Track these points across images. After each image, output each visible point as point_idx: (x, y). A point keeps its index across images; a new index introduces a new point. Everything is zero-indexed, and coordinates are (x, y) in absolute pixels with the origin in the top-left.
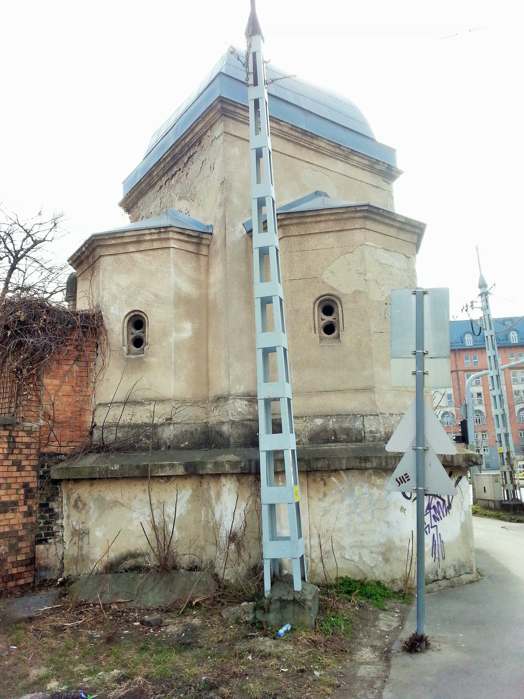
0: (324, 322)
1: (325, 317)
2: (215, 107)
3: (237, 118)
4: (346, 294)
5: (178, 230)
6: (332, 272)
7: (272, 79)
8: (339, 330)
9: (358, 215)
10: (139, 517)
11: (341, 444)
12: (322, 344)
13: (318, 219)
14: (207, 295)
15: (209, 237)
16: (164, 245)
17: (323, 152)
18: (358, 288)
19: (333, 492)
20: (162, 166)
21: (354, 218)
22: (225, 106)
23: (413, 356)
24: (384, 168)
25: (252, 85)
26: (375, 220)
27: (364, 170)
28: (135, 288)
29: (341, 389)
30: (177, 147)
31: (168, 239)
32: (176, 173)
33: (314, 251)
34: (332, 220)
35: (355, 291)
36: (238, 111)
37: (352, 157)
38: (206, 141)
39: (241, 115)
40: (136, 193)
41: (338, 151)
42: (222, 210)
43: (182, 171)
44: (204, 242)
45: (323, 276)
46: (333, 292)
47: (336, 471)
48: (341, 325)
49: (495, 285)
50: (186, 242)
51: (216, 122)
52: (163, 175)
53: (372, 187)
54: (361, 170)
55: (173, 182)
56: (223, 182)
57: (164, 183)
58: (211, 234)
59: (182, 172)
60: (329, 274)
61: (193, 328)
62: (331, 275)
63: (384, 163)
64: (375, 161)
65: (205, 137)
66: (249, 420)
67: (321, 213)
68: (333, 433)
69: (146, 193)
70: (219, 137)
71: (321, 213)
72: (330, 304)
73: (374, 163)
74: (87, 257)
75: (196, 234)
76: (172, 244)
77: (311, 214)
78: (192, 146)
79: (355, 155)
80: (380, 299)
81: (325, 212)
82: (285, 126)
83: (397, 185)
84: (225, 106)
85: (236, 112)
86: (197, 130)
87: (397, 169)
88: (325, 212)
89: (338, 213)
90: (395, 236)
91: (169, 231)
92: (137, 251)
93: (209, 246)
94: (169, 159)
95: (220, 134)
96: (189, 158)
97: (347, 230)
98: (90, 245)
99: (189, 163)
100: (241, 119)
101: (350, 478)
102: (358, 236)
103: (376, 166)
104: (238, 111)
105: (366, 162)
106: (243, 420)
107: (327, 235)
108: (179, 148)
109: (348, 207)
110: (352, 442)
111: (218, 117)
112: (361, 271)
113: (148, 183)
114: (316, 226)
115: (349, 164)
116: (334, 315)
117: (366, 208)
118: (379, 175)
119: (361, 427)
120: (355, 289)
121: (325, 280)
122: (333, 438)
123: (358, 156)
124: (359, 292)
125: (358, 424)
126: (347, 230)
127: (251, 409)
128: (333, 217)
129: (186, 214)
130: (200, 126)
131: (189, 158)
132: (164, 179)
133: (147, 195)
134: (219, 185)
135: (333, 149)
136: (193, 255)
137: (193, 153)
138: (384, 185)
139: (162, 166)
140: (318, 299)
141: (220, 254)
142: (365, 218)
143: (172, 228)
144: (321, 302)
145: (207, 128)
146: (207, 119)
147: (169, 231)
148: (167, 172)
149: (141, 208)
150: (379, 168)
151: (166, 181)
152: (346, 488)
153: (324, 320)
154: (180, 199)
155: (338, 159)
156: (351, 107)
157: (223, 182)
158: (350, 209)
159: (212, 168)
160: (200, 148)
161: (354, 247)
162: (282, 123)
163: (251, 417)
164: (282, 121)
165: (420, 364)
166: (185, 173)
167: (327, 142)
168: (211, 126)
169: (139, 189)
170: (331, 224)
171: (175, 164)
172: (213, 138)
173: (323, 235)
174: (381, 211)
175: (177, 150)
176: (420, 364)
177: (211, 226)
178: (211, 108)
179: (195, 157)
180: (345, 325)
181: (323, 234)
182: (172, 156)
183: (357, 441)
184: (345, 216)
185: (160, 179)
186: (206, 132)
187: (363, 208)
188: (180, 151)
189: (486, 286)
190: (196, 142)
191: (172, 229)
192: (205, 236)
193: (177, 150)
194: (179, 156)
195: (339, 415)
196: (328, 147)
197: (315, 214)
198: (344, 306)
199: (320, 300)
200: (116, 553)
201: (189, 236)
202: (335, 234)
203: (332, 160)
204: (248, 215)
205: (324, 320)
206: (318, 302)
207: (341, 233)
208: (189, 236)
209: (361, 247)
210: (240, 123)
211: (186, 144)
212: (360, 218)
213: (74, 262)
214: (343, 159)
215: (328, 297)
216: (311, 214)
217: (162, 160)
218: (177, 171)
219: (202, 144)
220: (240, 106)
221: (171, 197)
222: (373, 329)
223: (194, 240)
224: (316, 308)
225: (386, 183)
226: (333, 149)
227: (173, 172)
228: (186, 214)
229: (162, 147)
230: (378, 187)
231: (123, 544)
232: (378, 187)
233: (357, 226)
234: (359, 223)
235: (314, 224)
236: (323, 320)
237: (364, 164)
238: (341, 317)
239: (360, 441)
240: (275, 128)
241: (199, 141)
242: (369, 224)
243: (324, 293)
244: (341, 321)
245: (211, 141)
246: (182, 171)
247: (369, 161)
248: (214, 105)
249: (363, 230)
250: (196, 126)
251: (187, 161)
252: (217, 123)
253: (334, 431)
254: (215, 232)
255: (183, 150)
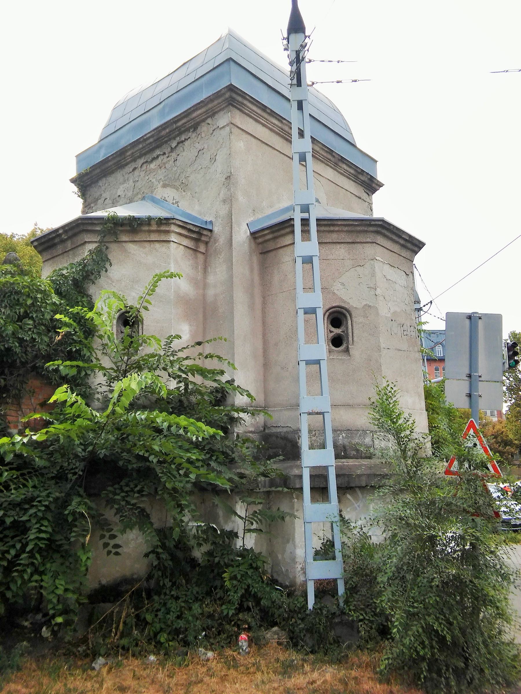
0: (332, 334)
1: (333, 329)
2: (224, 94)
3: (243, 109)
4: (356, 308)
5: (180, 223)
6: (343, 284)
7: (314, 81)
8: (348, 342)
9: (371, 229)
10: (137, 538)
11: (352, 460)
12: (331, 357)
13: (332, 228)
14: (204, 296)
15: (209, 233)
16: (163, 237)
17: (316, 156)
18: (368, 303)
19: (349, 510)
20: (141, 146)
21: (366, 231)
22: (234, 96)
23: (467, 378)
24: (366, 179)
25: (295, 85)
26: (385, 236)
27: (349, 179)
28: (128, 282)
29: (351, 403)
30: (164, 129)
31: (168, 232)
32: (158, 157)
33: (325, 261)
34: (345, 231)
35: (366, 305)
36: (245, 102)
37: (341, 164)
38: (204, 128)
39: (248, 107)
40: (98, 171)
41: (329, 157)
42: (227, 207)
43: (167, 155)
44: (203, 238)
45: (333, 287)
46: (343, 305)
47: (351, 488)
48: (350, 339)
49: (431, 302)
50: (186, 237)
51: (220, 110)
52: (140, 157)
53: (355, 197)
54: (346, 179)
55: (152, 166)
56: (230, 177)
57: (140, 166)
58: (211, 231)
59: (168, 157)
60: (340, 285)
61: (191, 331)
62: (342, 287)
63: (368, 174)
64: (360, 171)
65: (203, 124)
66: (251, 432)
67: (336, 223)
68: (343, 449)
69: (112, 172)
70: (223, 127)
71: (336, 223)
72: (339, 316)
73: (359, 173)
74: (63, 241)
75: (197, 230)
76: (173, 237)
77: (326, 223)
78: (185, 131)
79: (344, 163)
80: (386, 315)
81: (339, 223)
82: (286, 125)
83: (376, 197)
84: (234, 96)
85: (243, 104)
86: (194, 115)
87: (378, 181)
88: (339, 223)
89: (352, 225)
90: (398, 253)
91: (171, 223)
92: (130, 241)
93: (207, 243)
94: (151, 140)
95: (225, 124)
96: (178, 143)
97: (358, 243)
98: (72, 228)
99: (178, 148)
100: (247, 112)
101: (365, 495)
102: (369, 250)
103: (360, 176)
104: (245, 102)
105: (352, 171)
106: (246, 432)
107: (338, 246)
108: (167, 130)
109: (362, 220)
110: (362, 458)
111: (224, 105)
112: (372, 286)
113: (117, 162)
114: (329, 235)
115: (337, 171)
116: (343, 328)
117: (380, 223)
118: (361, 185)
119: (371, 443)
120: (364, 303)
121: (336, 291)
122: (343, 454)
123: (346, 164)
124: (370, 306)
125: (368, 440)
126: (358, 243)
127: (253, 420)
128: (346, 229)
129: (173, 203)
130: (199, 112)
131: (178, 143)
132: (142, 161)
133: (113, 175)
134: (223, 179)
135: (325, 154)
136: (191, 252)
137: (185, 139)
138: (364, 196)
139: (141, 146)
140: (328, 310)
141: (223, 255)
142: (378, 232)
143: (175, 220)
144: (330, 314)
145: (208, 115)
146: (210, 106)
147: (171, 223)
148: (145, 154)
149: (103, 188)
150: (362, 178)
151: (143, 163)
152: (361, 506)
153: (333, 332)
154: (165, 186)
155: (328, 165)
156: (336, 110)
157: (230, 177)
158: (364, 222)
159: (213, 160)
160: (194, 135)
161: (365, 261)
162: (284, 121)
163: (253, 430)
164: (285, 119)
165: (473, 387)
166: (172, 159)
167: (321, 146)
168: (212, 114)
169: (103, 168)
170: (343, 235)
171: (157, 147)
172: (215, 127)
173: (334, 246)
174: (392, 227)
175: (164, 133)
176: (473, 387)
177: (211, 222)
178: (218, 95)
179: (187, 143)
180: (355, 339)
181: (334, 245)
182: (155, 138)
183: (366, 458)
184: (359, 228)
185: (135, 160)
186: (206, 119)
187: (377, 223)
188: (167, 133)
189: (419, 302)
190: (190, 127)
191: (174, 221)
192: (205, 232)
193: (164, 133)
194: (166, 139)
195: (348, 430)
196: (321, 152)
197: (329, 223)
198: (354, 319)
199: (330, 311)
200: (108, 580)
201: (190, 230)
202: (345, 245)
203: (323, 165)
204: (251, 215)
205: (333, 332)
206: (328, 314)
207: (353, 245)
208: (190, 230)
209: (372, 262)
210: (245, 116)
211: (177, 128)
212: (372, 232)
213: (41, 244)
214: (333, 166)
215: (338, 309)
216: (326, 223)
217: (142, 140)
218: (160, 155)
219: (198, 131)
220: (248, 97)
221: (150, 183)
222: (383, 345)
223: (194, 236)
224: (326, 319)
225: (367, 195)
226: (325, 154)
227: (155, 155)
228: (173, 203)
229: (142, 125)
230: (360, 198)
231: (117, 569)
232: (360, 198)
233: (369, 240)
234: (370, 238)
235: (327, 234)
236: (331, 332)
237: (350, 173)
238: (350, 331)
239: (370, 458)
240: (277, 126)
241: (195, 127)
242: (380, 240)
243: (334, 305)
244: (350, 334)
245: (212, 129)
246: (167, 155)
247: (356, 170)
248: (222, 92)
249: (375, 244)
250: (194, 111)
251: (176, 147)
252: (222, 113)
253: (344, 447)
254: (216, 229)
255: (173, 134)
